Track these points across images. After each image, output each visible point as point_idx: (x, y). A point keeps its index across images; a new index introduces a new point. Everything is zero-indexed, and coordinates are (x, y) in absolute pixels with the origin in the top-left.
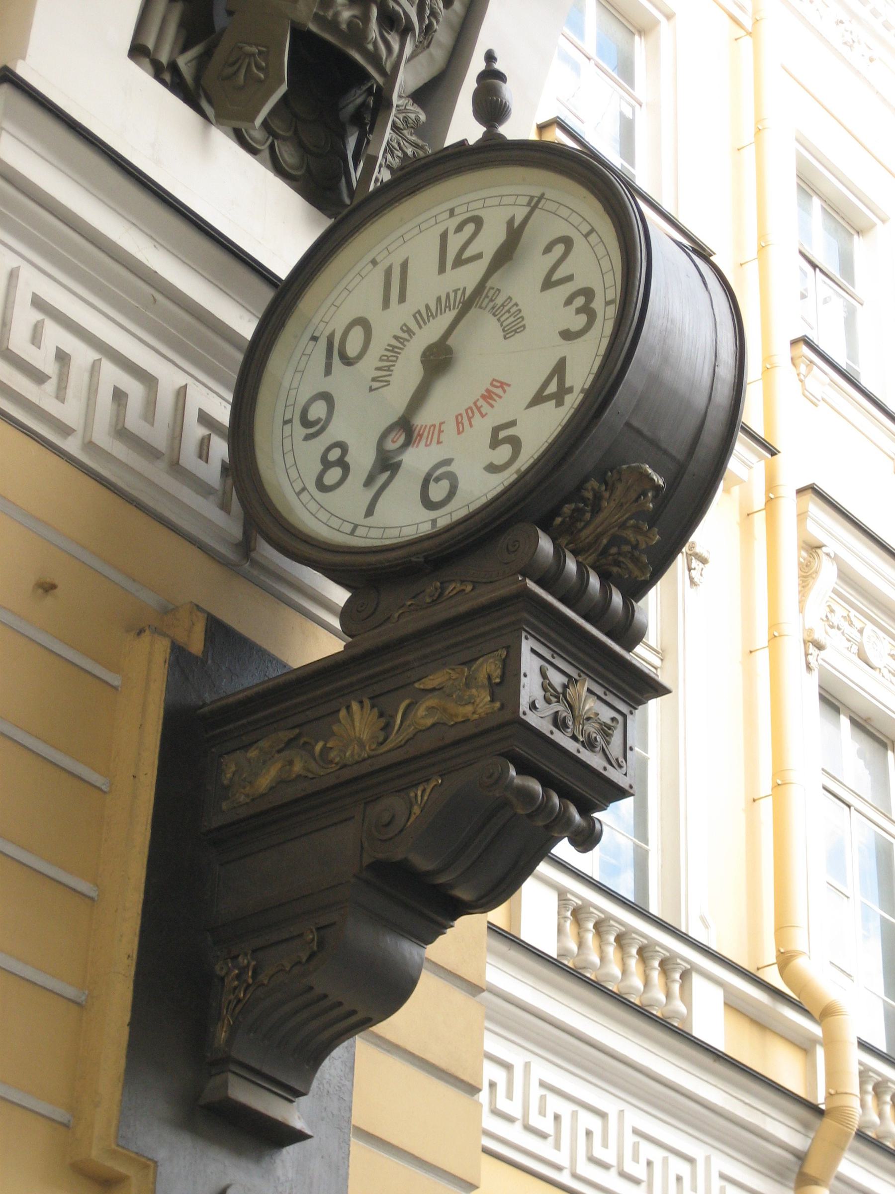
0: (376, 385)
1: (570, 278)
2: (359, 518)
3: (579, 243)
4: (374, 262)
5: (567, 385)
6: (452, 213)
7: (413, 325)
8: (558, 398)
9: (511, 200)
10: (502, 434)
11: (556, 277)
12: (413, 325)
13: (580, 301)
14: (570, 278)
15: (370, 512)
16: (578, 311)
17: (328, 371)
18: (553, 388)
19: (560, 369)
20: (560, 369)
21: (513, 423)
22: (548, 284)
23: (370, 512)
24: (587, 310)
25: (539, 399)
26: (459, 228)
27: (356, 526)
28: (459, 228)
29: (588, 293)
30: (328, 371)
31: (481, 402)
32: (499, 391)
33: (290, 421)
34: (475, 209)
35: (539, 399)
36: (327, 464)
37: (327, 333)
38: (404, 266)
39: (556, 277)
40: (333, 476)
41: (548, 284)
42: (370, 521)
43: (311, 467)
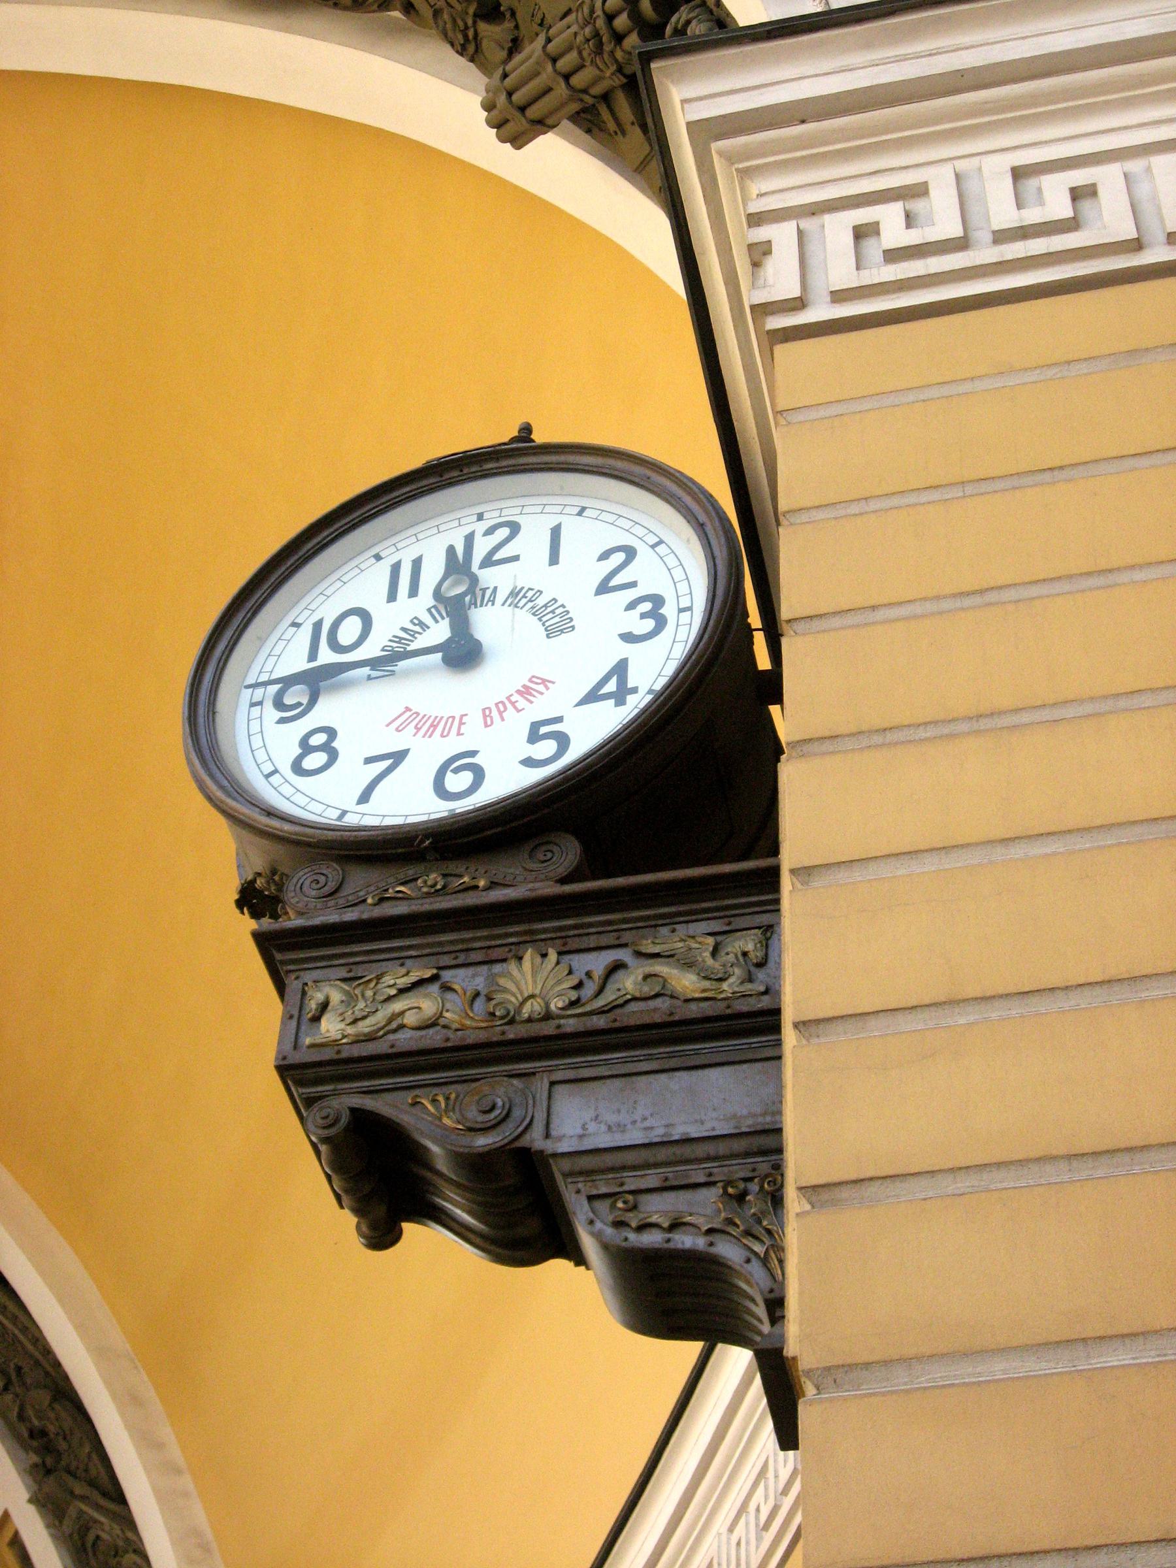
1: (633, 584)
2: (350, 803)
6: (480, 517)
8: (620, 697)
10: (544, 730)
13: (646, 606)
14: (633, 584)
15: (365, 797)
16: (643, 616)
18: (611, 686)
19: (621, 669)
20: (621, 669)
21: (559, 720)
22: (604, 588)
23: (365, 797)
25: (593, 697)
26: (490, 531)
28: (490, 531)
29: (657, 601)
32: (541, 688)
34: (511, 514)
36: (306, 748)
37: (315, 618)
40: (314, 760)
41: (604, 588)
42: (363, 808)
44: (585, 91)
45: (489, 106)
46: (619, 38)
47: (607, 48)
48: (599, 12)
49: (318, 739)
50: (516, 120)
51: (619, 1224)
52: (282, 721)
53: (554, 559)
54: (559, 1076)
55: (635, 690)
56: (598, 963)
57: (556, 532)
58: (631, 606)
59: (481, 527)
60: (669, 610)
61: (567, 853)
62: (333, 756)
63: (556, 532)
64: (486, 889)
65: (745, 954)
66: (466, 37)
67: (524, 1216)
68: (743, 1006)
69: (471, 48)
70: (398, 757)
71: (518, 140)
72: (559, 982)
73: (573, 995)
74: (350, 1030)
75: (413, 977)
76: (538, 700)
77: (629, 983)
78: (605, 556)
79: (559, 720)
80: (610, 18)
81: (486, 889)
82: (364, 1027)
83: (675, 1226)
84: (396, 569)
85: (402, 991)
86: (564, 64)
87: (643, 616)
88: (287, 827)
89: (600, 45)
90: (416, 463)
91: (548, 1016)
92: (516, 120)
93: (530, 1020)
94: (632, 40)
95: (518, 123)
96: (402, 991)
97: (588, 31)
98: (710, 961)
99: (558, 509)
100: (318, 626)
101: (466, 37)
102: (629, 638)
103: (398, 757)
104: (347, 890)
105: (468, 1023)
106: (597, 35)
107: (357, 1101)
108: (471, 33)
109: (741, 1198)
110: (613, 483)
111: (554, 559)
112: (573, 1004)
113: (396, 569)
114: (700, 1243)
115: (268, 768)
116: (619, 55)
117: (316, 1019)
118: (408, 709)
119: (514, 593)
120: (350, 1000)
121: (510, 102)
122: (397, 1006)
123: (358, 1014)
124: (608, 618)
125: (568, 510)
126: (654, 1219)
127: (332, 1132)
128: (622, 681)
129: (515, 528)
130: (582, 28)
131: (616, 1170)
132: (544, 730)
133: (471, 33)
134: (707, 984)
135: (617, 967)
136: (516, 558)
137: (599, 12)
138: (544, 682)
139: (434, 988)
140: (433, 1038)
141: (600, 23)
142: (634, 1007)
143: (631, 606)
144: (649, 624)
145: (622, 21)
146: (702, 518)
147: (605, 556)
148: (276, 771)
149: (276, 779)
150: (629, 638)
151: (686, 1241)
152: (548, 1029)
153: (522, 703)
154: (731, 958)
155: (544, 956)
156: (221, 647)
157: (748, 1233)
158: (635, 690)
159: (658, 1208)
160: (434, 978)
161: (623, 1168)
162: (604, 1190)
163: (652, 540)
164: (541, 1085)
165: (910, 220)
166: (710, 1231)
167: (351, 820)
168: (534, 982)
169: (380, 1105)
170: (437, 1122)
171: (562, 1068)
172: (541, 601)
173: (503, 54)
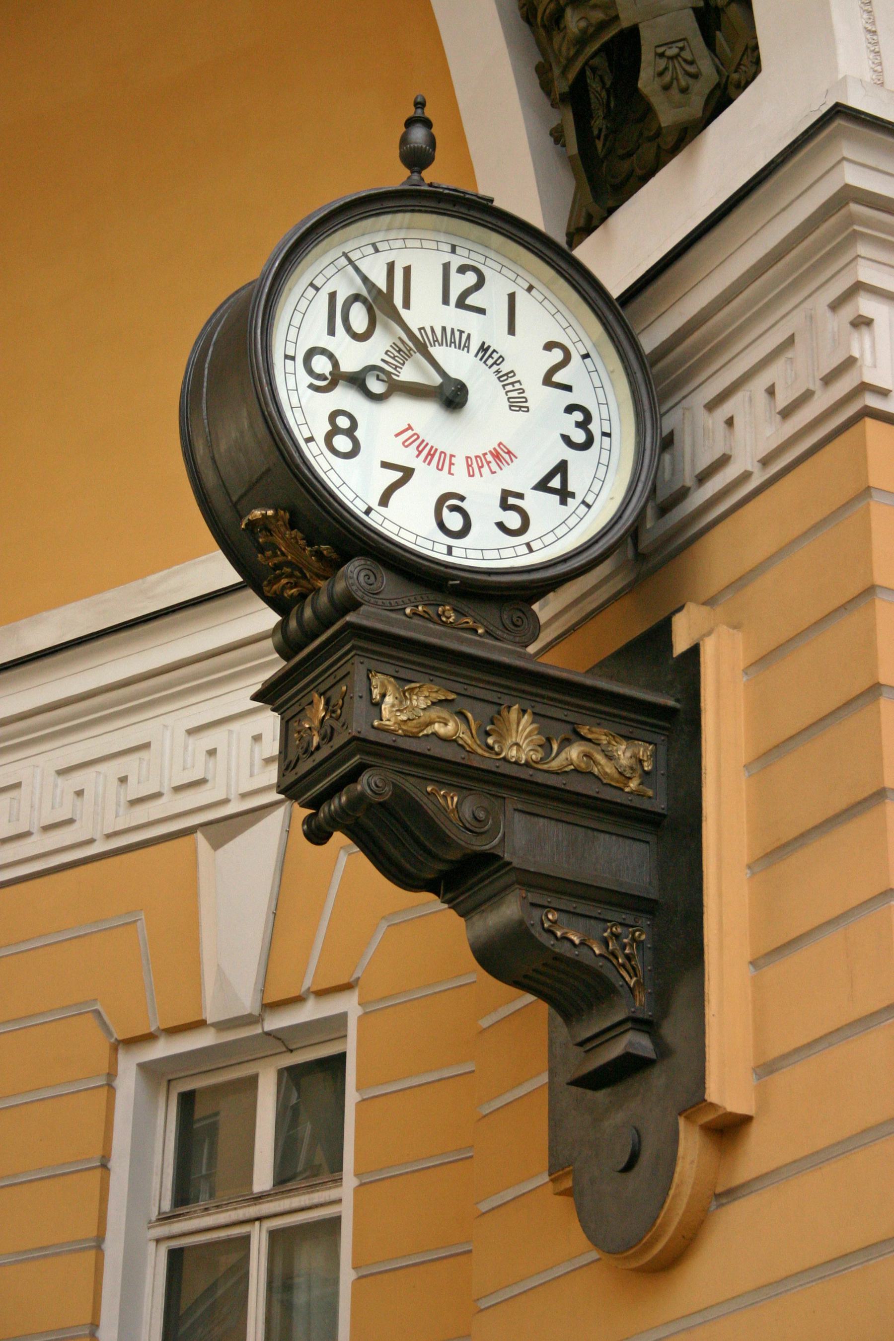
1: (568, 388)
2: (374, 503)
5: (570, 489)
6: (453, 250)
10: (511, 501)
15: (384, 501)
16: (578, 425)
17: (331, 332)
19: (562, 468)
20: (562, 468)
21: (520, 496)
23: (384, 501)
24: (583, 425)
25: (543, 486)
26: (462, 269)
29: (588, 417)
31: (489, 457)
32: (506, 457)
34: (476, 260)
38: (407, 271)
39: (398, 475)
42: (382, 509)
53: (512, 331)
55: (572, 495)
57: (512, 297)
58: (570, 409)
59: (456, 262)
60: (594, 427)
63: (512, 297)
70: (408, 473)
76: (506, 468)
78: (549, 346)
87: (578, 425)
102: (567, 439)
103: (408, 473)
111: (512, 331)
118: (410, 428)
144: (579, 436)
147: (549, 346)
157: (623, 966)
158: (572, 495)
172: (505, 368)
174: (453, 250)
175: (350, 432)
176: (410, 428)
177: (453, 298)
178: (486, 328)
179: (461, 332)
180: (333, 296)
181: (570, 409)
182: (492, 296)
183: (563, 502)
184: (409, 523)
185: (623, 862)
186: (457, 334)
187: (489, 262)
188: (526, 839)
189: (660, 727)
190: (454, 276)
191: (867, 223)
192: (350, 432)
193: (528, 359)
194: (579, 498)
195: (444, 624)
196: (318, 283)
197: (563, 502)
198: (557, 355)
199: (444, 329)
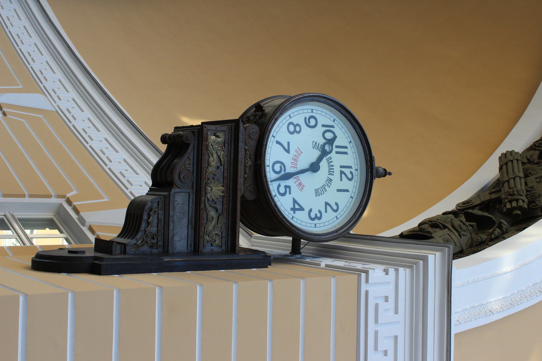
0: (314, 143)
1: (326, 212)
2: (277, 139)
3: (336, 214)
4: (350, 142)
5: (296, 212)
6: (356, 170)
7: (331, 177)
8: (294, 209)
9: (326, 224)
10: (288, 189)
11: (287, 148)
12: (331, 177)
13: (319, 215)
14: (326, 212)
15: (278, 142)
16: (316, 215)
17: (323, 126)
18: (297, 207)
19: (302, 209)
20: (302, 209)
21: (290, 193)
22: (327, 204)
23: (278, 142)
24: (316, 217)
25: (295, 202)
26: (351, 173)
27: (336, 217)
28: (351, 173)
29: (320, 218)
30: (323, 126)
31: (299, 181)
32: (300, 188)
33: (312, 112)
34: (355, 178)
35: (295, 202)
36: (295, 126)
37: (335, 126)
38: (346, 153)
39: (287, 148)
40: (292, 128)
41: (327, 204)
42: (275, 142)
43: (295, 121)
44: (503, 186)
45: (511, 153)
46: (511, 202)
47: (509, 197)
48: (519, 197)
49: (298, 129)
50: (506, 160)
51: (151, 210)
52: (305, 118)
53: (339, 190)
54: (191, 194)
55: (294, 213)
56: (219, 206)
57: (347, 191)
58: (320, 212)
59: (353, 170)
60: (316, 221)
61: (250, 197)
62: (292, 133)
63: (347, 191)
64: (244, 176)
65: (215, 241)
66: (537, 146)
67: (162, 177)
68: (202, 240)
69: (533, 147)
70: (288, 151)
71: (500, 158)
72: (215, 196)
73: (211, 200)
74: (210, 144)
75: (222, 159)
76: (297, 187)
77: (212, 213)
78: (337, 204)
79: (290, 193)
80: (517, 200)
81: (244, 176)
82: (210, 147)
83: (148, 223)
84: (346, 147)
85: (219, 156)
86: (512, 181)
87: (316, 215)
88: (270, 127)
89: (511, 195)
90: (374, 154)
91: (206, 194)
92: (506, 160)
93: (206, 189)
94: (508, 206)
95: (505, 161)
96: (219, 156)
97: (516, 193)
98: (214, 233)
99: (354, 191)
100: (333, 127)
101: (537, 146)
102: (310, 211)
103: (288, 151)
104: (250, 141)
105: (207, 174)
106: (514, 195)
107: (192, 145)
108: (538, 148)
109: (153, 238)
110: (357, 207)
111: (339, 190)
112: (208, 200)
113: (346, 147)
114: (142, 228)
115: (292, 116)
116: (506, 200)
117: (215, 135)
118: (302, 153)
119: (331, 180)
120: (218, 143)
121: (509, 161)
122: (215, 156)
123: (214, 146)
124: (317, 204)
125: (353, 194)
126: (151, 218)
127: (184, 137)
128: (298, 210)
129: (350, 180)
130: (517, 191)
131: (166, 205)
132: (288, 189)
133: (538, 148)
134: (208, 232)
135: (217, 210)
136: (341, 180)
137: (519, 197)
138: (302, 189)
139: (219, 164)
140: (204, 165)
141: (516, 197)
142: (205, 213)
143: (320, 212)
144: (313, 216)
145: (514, 204)
146: (339, 232)
147: (337, 204)
148: (290, 117)
149: (288, 117)
150: (310, 211)
151: (143, 225)
152: (203, 193)
153: (297, 183)
154: (214, 238)
155: (223, 192)
156: (331, 102)
157: (143, 240)
158: (294, 213)
159: (154, 219)
160: (221, 164)
161: (164, 210)
162: (160, 205)
163: (338, 217)
164: (190, 190)
165: (387, 310)
166: (145, 231)
167: (271, 139)
168: (215, 191)
169: (191, 148)
170: (185, 164)
171: (193, 196)
172: (326, 187)
173: (529, 157)
174: (356, 170)
175: (295, 131)
176: (302, 153)
177: (343, 170)
178: (337, 184)
179: (333, 172)
180: (333, 127)
181: (320, 212)
182: (345, 184)
183: (292, 209)
184: (273, 154)
185: (180, 239)
186: (332, 170)
187: (356, 183)
188: (181, 200)
189: (228, 248)
190: (349, 170)
191: (417, 268)
192: (295, 131)
193: (331, 196)
194: (294, 215)
195: (245, 162)
196: (314, 226)
197: (292, 209)
198: (335, 207)
199: (333, 166)
